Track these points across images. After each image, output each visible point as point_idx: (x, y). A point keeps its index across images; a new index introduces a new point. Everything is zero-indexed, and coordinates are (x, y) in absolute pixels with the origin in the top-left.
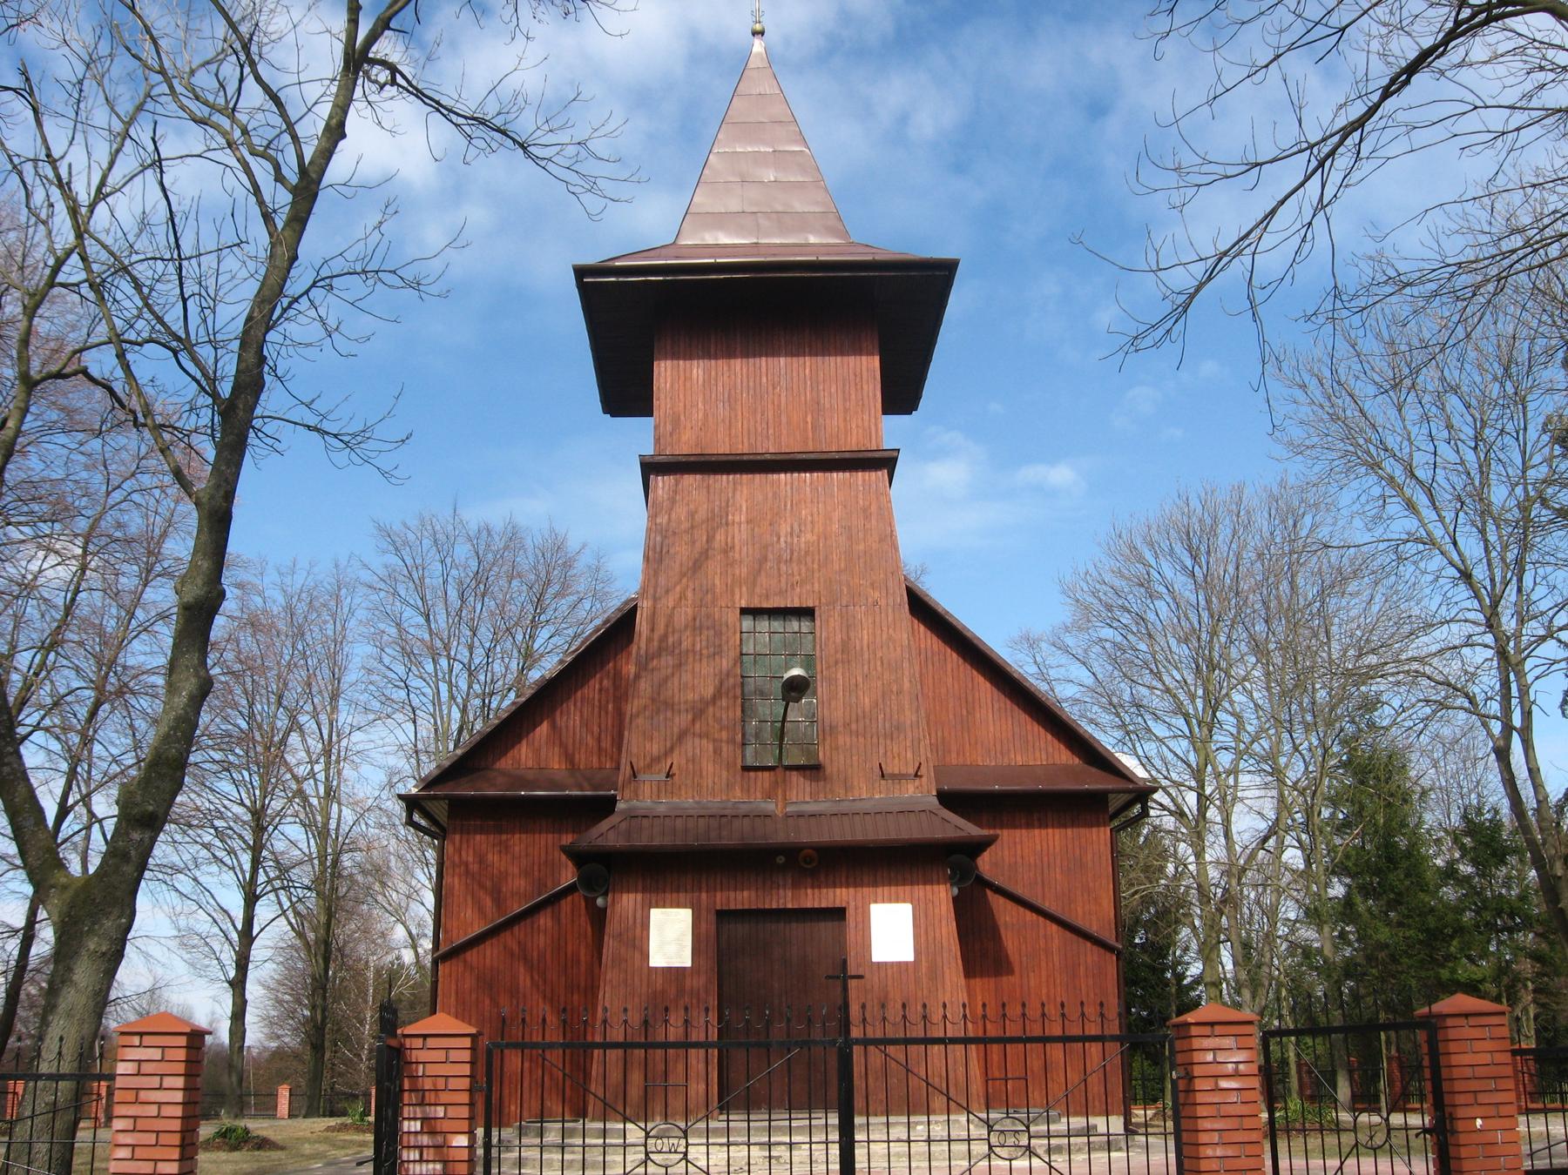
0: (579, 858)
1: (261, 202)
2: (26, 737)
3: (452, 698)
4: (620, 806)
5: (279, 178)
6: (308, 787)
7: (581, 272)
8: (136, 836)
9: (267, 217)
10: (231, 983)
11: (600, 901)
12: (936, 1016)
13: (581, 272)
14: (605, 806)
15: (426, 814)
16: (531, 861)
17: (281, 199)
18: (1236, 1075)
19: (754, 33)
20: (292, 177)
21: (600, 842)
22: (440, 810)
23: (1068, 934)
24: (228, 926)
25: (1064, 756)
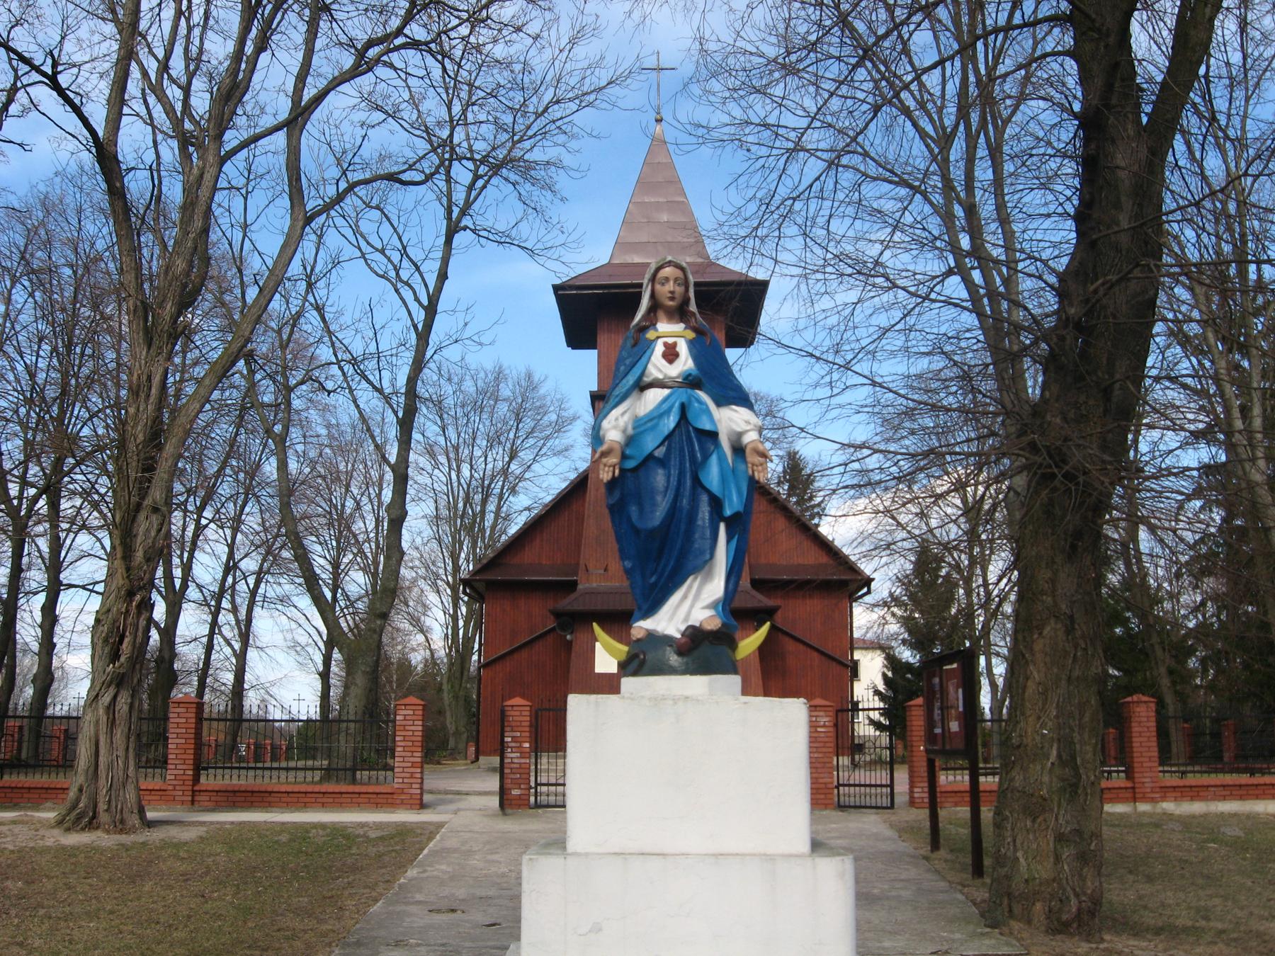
0: (558, 615)
1: (412, 320)
2: (206, 526)
3: (459, 483)
4: (580, 587)
5: (417, 299)
6: (366, 547)
7: (556, 288)
8: (378, 622)
9: (415, 327)
10: (320, 674)
11: (568, 637)
12: (20, 708)
13: (556, 288)
14: (572, 586)
15: (472, 588)
16: (534, 614)
17: (420, 315)
18: (824, 726)
19: (657, 121)
20: (425, 303)
21: (569, 608)
22: (481, 587)
23: (823, 658)
24: (317, 638)
25: (824, 559)
